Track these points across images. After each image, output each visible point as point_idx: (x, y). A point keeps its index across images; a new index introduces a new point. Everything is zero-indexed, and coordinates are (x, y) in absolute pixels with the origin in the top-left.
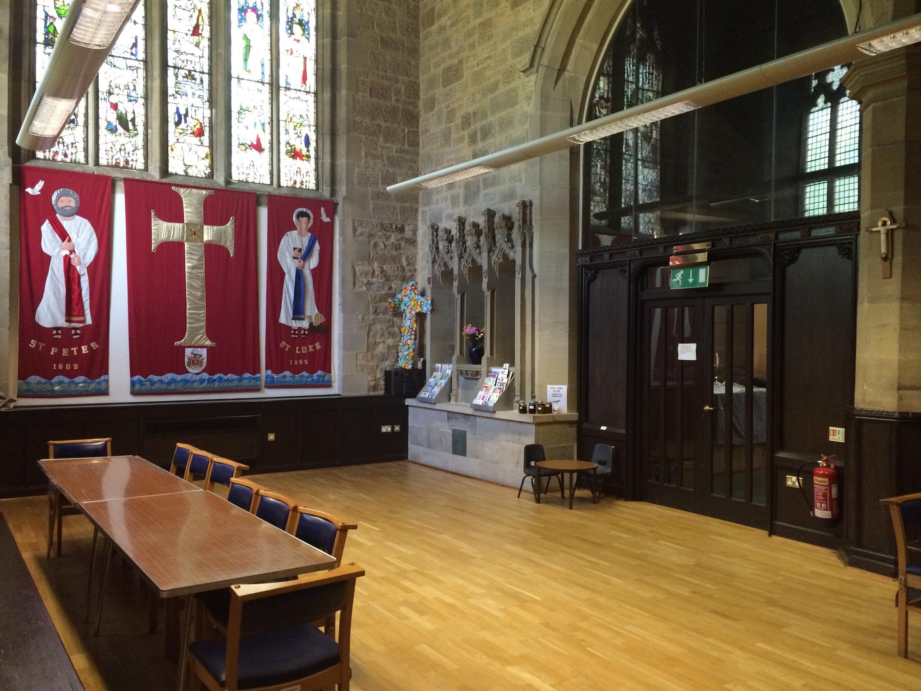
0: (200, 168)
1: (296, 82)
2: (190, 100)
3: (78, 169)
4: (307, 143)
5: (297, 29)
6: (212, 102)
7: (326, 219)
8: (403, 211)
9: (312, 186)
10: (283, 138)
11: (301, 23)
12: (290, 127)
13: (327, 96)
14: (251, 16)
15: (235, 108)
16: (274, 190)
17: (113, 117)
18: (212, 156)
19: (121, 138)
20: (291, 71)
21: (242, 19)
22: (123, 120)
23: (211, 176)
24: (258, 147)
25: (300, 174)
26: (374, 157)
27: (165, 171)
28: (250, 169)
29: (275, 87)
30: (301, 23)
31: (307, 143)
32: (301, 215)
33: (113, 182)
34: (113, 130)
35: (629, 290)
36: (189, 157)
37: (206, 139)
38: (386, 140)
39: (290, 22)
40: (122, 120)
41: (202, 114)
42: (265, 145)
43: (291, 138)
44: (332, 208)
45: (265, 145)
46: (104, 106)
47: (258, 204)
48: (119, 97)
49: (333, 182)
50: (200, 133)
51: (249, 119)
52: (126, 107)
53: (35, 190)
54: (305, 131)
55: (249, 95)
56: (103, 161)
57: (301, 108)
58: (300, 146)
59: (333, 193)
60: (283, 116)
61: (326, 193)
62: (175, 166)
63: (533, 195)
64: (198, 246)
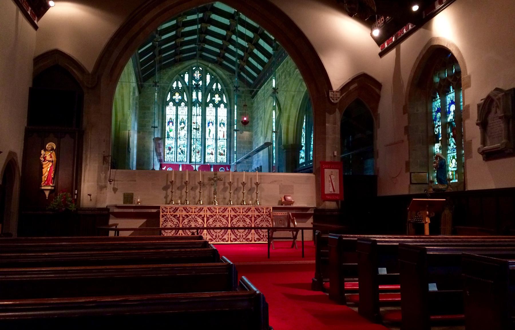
0: (198, 160)
1: (221, 137)
2: (197, 146)
3: (173, 163)
4: (224, 151)
5: (222, 125)
6: (201, 145)
7: (228, 170)
8: (248, 166)
9: (225, 161)
10: (218, 151)
11: (223, 124)
12: (220, 148)
13: (229, 140)
14: (211, 124)
15: (207, 146)
16: (215, 164)
17: (180, 151)
18: (201, 157)
19: (182, 155)
20: (220, 135)
21: (209, 126)
22: (182, 152)
23: (201, 162)
24: (212, 154)
25: (223, 159)
26: (240, 154)
27: (190, 162)
28: (210, 159)
29: (216, 140)
30: (223, 124)
31: (224, 151)
32: (221, 169)
33: (179, 165)
34: (180, 154)
35: (84, 176)
36: (197, 158)
37: (200, 153)
38: (243, 149)
39: (220, 124)
40: (182, 152)
41: (200, 148)
42: (214, 153)
43: (220, 151)
44: (229, 167)
45: (214, 153)
46: (178, 149)
47: (211, 167)
48: (181, 147)
49: (230, 161)
50: (198, 152)
51: (210, 148)
52: (183, 149)
53: (164, 169)
54: (224, 149)
55: (210, 142)
56: (178, 160)
57: (223, 143)
58: (222, 152)
59: (230, 163)
60: (218, 146)
61: (228, 164)
62: (193, 160)
63: (262, 164)
64: (308, 178)
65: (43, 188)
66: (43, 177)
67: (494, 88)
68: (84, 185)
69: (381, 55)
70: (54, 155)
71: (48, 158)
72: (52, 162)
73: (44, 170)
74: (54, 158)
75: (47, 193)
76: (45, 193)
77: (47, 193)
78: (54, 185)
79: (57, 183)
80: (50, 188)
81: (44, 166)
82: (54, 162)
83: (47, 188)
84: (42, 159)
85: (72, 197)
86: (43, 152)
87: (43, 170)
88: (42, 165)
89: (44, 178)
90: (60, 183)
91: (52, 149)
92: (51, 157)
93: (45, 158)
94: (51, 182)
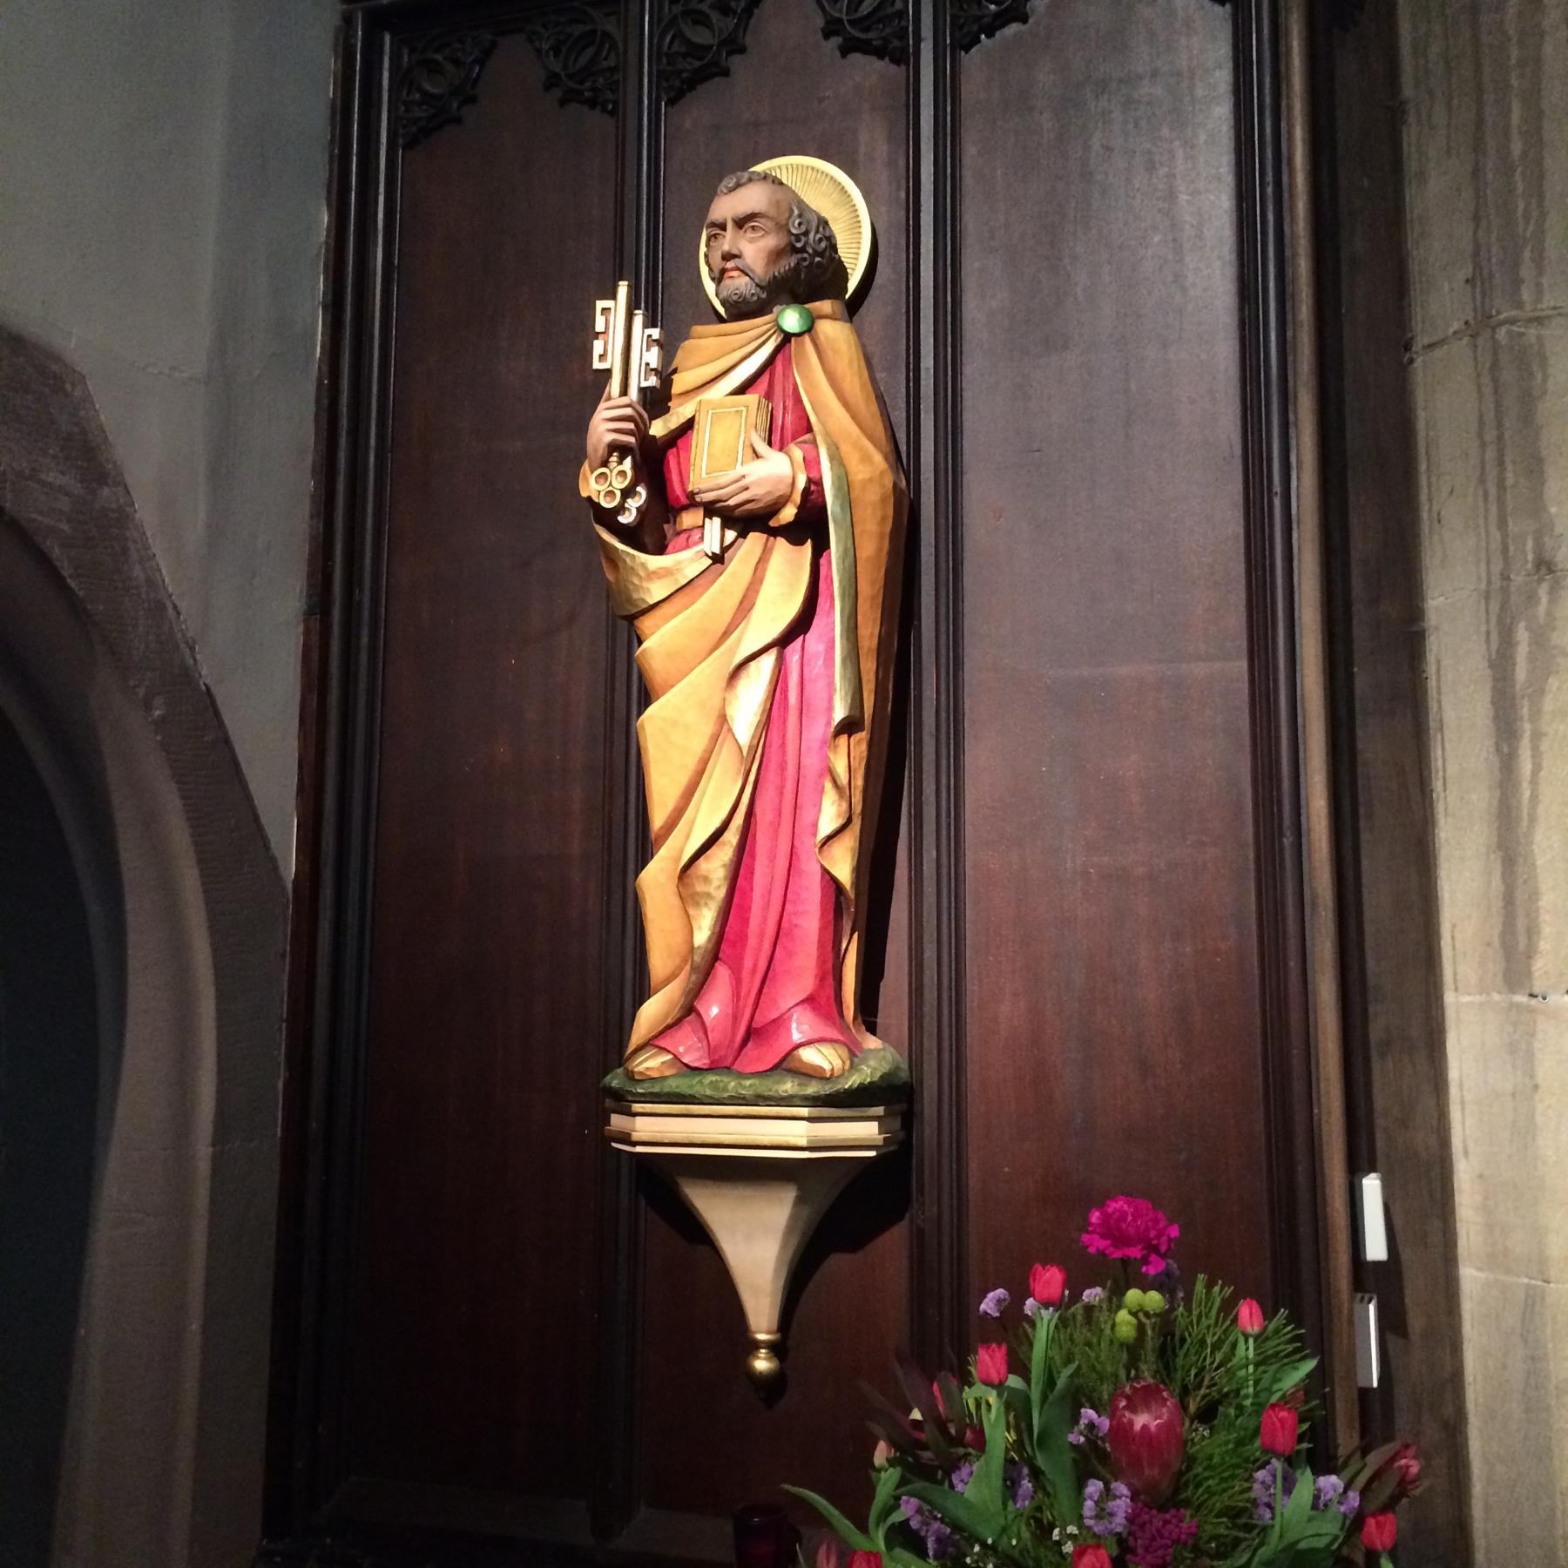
65: (653, 1129)
66: (656, 879)
67: (824, 214)
68: (1519, 1049)
69: (1310, 1519)
70: (833, 362)
71: (731, 454)
72: (809, 526)
73: (669, 735)
74: (849, 457)
75: (754, 1244)
76: (698, 1235)
77: (754, 1244)
78: (878, 1057)
79: (942, 1024)
80: (790, 1133)
81: (660, 642)
82: (860, 538)
83: (745, 1112)
84: (607, 484)
85: (1318, 1332)
86: (618, 336)
87: (654, 724)
88: (626, 623)
89: (674, 917)
90: (998, 1006)
91: (808, 273)
92: (788, 427)
93: (654, 460)
94: (824, 1001)
